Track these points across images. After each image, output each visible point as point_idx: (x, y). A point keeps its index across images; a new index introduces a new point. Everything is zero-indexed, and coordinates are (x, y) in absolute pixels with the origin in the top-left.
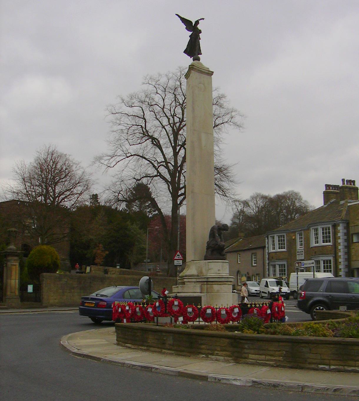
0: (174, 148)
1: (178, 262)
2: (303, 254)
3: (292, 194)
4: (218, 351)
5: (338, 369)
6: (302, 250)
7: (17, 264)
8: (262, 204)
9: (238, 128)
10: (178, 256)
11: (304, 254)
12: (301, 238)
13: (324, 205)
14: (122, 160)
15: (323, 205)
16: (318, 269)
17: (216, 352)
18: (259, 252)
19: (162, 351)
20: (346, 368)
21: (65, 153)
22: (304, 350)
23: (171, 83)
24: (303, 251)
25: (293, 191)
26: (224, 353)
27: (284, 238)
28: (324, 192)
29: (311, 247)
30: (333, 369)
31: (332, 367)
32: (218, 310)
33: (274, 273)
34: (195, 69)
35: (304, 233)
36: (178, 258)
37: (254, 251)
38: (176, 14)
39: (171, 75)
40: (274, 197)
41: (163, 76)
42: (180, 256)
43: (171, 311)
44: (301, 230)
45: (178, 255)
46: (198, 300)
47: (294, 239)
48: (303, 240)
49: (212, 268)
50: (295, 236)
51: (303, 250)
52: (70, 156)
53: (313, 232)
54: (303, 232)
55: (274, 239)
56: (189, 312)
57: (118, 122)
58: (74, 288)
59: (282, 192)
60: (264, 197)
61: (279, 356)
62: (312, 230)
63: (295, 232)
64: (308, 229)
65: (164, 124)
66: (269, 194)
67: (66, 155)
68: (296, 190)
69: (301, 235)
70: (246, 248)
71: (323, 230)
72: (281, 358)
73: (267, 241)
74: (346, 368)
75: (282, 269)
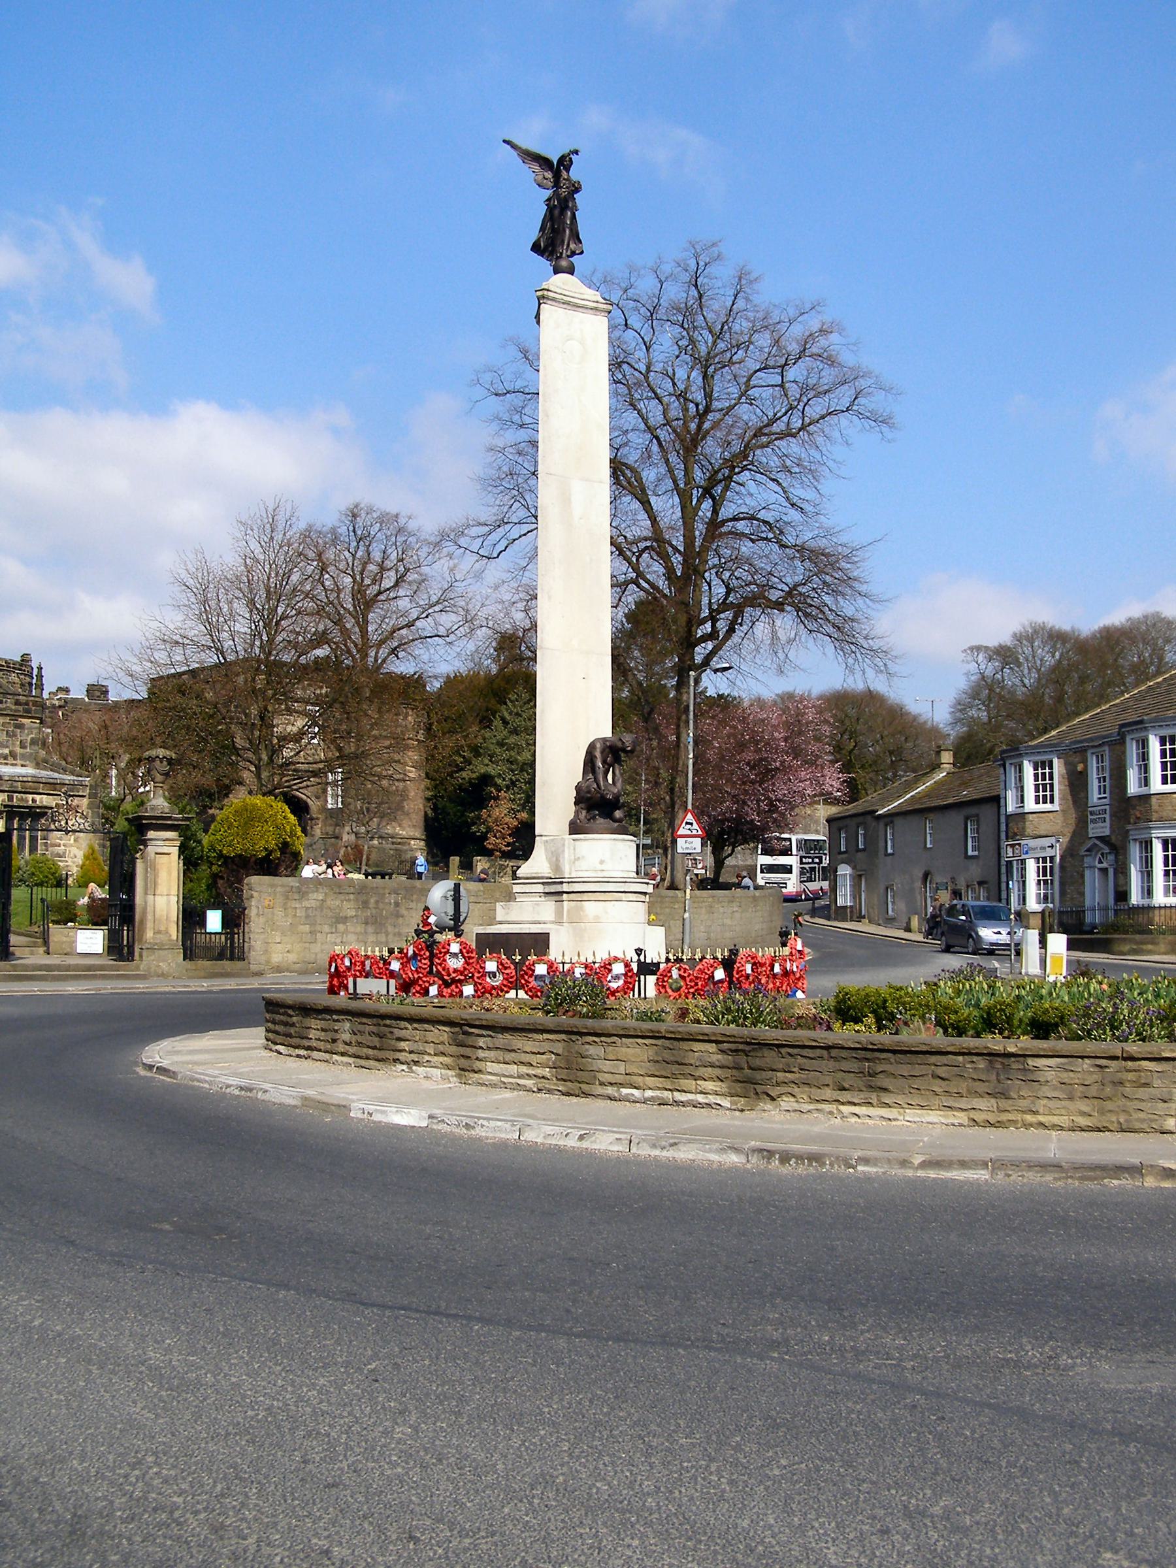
0: (684, 497)
1: (688, 845)
3: (1155, 624)
4: (429, 1054)
5: (659, 1098)
7: (175, 851)
8: (1050, 661)
9: (877, 429)
10: (689, 826)
11: (1111, 819)
12: (1103, 770)
14: (525, 535)
16: (1147, 867)
17: (427, 1058)
18: (987, 812)
19: (331, 1058)
20: (679, 1096)
21: (394, 512)
22: (592, 1050)
23: (675, 292)
24: (1108, 812)
25: (1157, 615)
26: (442, 1059)
27: (1051, 767)
30: (652, 1099)
31: (649, 1093)
32: (567, 967)
34: (554, 300)
36: (689, 833)
37: (973, 810)
38: (504, 141)
39: (667, 268)
40: (1094, 636)
41: (642, 272)
42: (695, 826)
43: (444, 969)
44: (1100, 745)
45: (687, 823)
46: (540, 942)
47: (1080, 772)
48: (1107, 775)
49: (583, 857)
50: (1085, 762)
51: (1107, 807)
52: (410, 518)
53: (1132, 751)
54: (1106, 748)
55: (1146, 772)
56: (489, 973)
57: (516, 418)
58: (344, 920)
59: (1123, 620)
60: (1056, 638)
61: (543, 1065)
63: (1086, 750)
64: (1122, 742)
65: (651, 422)
66: (1072, 627)
67: (397, 516)
68: (1157, 610)
69: (1100, 759)
70: (950, 801)
71: (1163, 743)
72: (546, 1072)
73: (1002, 777)
74: (679, 1096)
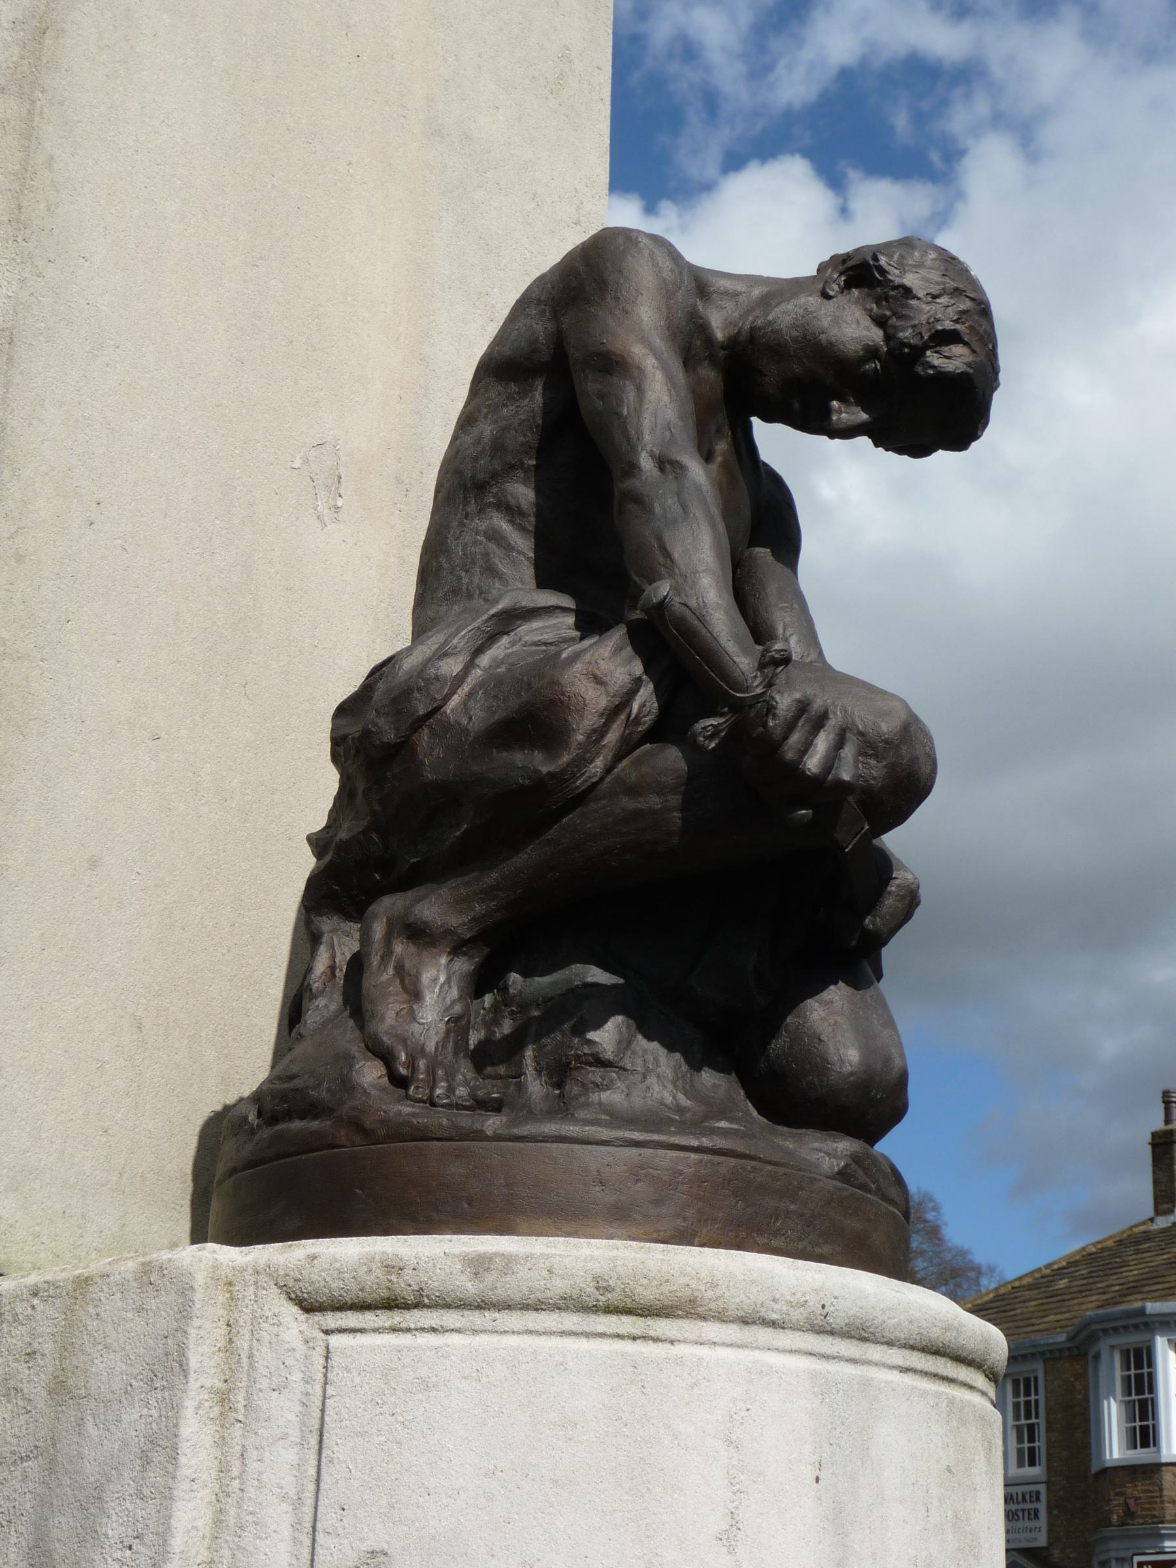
2: (1043, 1514)
6: (1034, 1488)
11: (1049, 1513)
13: (1158, 1211)
15: (1149, 1210)
28: (1154, 1135)
29: (1095, 1469)
33: (1023, 1422)
35: (1046, 1373)
51: (1042, 1488)
62: (1104, 1356)
75: (1034, 1441)
